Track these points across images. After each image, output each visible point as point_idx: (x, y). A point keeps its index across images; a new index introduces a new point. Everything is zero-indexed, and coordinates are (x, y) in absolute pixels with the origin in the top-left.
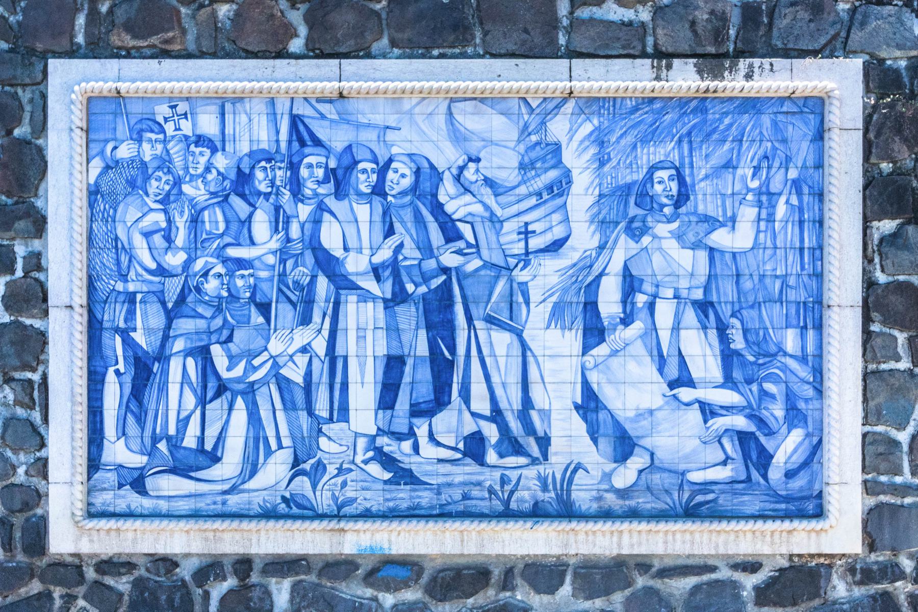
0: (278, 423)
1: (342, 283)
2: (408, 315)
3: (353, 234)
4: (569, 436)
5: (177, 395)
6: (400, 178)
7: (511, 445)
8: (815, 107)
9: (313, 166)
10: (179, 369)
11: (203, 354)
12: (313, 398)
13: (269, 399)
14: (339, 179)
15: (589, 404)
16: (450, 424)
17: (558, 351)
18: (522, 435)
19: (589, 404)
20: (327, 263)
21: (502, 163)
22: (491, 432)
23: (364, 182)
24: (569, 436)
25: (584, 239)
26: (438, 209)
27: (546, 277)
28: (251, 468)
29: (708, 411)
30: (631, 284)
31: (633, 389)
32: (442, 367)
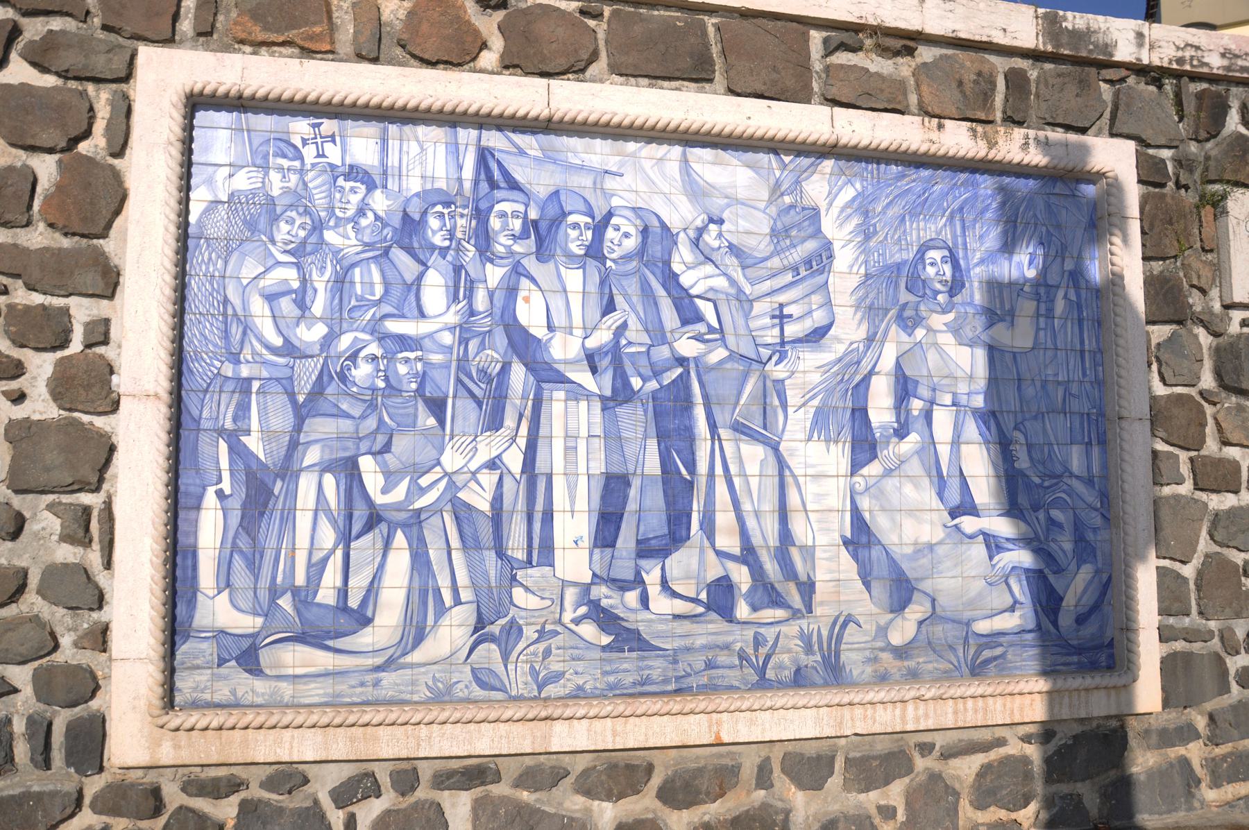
0: (455, 570)
1: (546, 375)
2: (633, 420)
3: (561, 309)
4: (833, 570)
5: (309, 524)
6: (622, 239)
7: (767, 594)
8: (1228, 691)
9: (507, 214)
10: (312, 490)
11: (349, 471)
12: (506, 533)
13: (442, 534)
14: (543, 233)
15: (860, 538)
16: (689, 566)
17: (820, 463)
18: (778, 578)
19: (860, 538)
20: (523, 345)
21: (751, 226)
22: (741, 576)
23: (575, 240)
24: (833, 570)
25: (849, 329)
26: (671, 280)
27: (807, 371)
28: (415, 632)
29: (993, 545)
30: (904, 387)
31: (911, 520)
32: (677, 489)
